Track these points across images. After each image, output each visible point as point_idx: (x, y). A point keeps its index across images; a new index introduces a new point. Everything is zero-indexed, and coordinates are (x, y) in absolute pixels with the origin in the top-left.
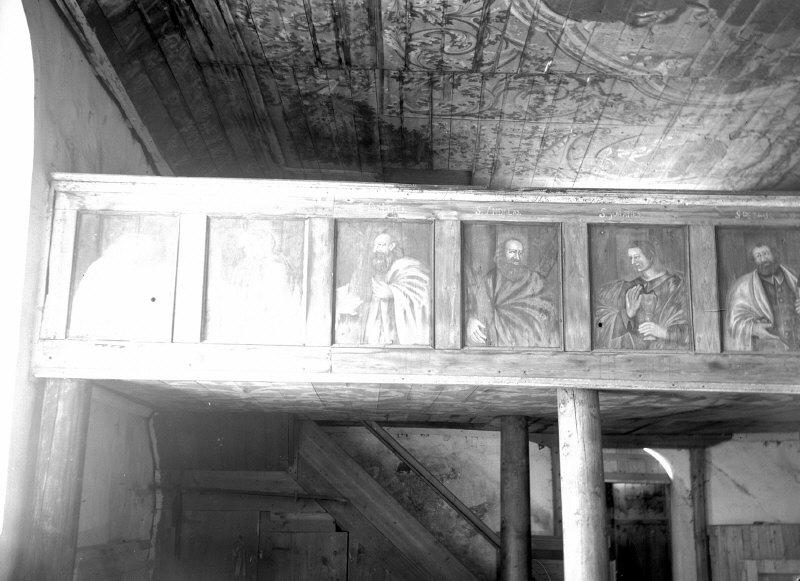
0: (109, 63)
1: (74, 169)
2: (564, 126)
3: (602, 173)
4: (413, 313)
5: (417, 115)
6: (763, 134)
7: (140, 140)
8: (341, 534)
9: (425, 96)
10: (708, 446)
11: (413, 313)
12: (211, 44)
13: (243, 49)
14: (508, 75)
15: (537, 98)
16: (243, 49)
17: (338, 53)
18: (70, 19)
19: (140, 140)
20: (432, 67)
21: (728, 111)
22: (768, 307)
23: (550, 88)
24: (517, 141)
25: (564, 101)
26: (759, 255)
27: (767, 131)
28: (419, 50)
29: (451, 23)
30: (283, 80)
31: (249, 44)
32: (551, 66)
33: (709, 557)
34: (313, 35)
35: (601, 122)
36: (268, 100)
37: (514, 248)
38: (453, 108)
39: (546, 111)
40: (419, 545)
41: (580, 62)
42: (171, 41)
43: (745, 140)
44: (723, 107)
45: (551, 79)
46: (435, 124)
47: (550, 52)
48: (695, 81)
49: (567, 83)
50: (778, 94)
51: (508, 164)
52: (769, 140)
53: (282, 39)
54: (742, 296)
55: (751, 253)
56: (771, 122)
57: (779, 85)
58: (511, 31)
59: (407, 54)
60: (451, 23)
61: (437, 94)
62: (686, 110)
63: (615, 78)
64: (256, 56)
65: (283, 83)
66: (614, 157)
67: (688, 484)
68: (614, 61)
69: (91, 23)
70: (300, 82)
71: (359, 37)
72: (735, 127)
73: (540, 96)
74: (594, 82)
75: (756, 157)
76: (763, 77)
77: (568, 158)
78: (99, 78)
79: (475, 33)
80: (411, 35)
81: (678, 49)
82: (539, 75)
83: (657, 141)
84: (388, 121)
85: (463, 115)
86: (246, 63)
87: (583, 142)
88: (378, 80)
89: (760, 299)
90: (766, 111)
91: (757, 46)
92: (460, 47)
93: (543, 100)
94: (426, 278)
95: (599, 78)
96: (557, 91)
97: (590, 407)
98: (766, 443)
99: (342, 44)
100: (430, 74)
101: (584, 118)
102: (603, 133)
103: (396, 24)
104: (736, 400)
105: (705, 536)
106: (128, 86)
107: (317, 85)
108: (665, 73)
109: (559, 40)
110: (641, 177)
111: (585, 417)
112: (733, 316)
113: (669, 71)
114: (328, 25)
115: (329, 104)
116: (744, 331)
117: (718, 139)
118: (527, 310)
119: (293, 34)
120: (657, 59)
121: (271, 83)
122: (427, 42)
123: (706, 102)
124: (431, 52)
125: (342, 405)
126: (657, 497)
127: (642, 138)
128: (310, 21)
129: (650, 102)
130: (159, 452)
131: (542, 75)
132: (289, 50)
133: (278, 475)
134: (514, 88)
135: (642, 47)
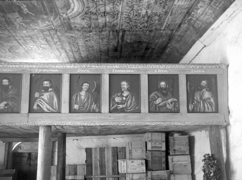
98: (73, 140)
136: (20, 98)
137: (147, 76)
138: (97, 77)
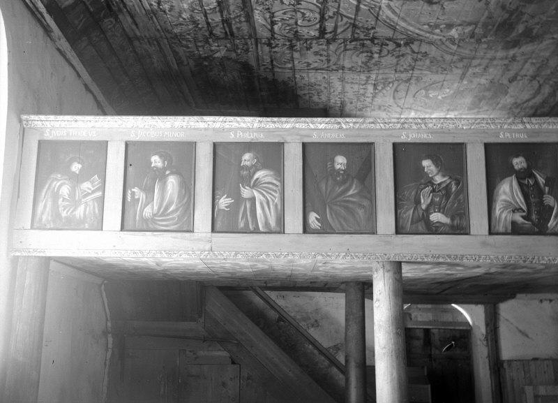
0: (65, 39)
1: (39, 113)
2: (389, 76)
3: (420, 108)
4: (270, 212)
5: (284, 71)
6: (534, 78)
7: (91, 92)
8: (235, 366)
9: (288, 56)
10: (498, 303)
11: (270, 212)
12: (136, 25)
13: (159, 27)
14: (345, 40)
15: (367, 56)
16: (159, 27)
17: (224, 28)
18: (34, 10)
19: (91, 92)
20: (291, 35)
21: (506, 62)
22: (523, 201)
23: (376, 49)
24: (356, 87)
25: (386, 58)
26: (517, 164)
27: (536, 76)
28: (280, 24)
29: (300, 4)
30: (188, 47)
31: (162, 23)
32: (374, 33)
33: (500, 383)
34: (206, 16)
35: (415, 72)
36: (180, 62)
37: (340, 161)
38: (309, 64)
39: (375, 65)
40: (291, 374)
41: (395, 30)
42: (108, 23)
43: (521, 82)
44: (502, 59)
45: (376, 42)
46: (297, 76)
47: (373, 23)
48: (479, 41)
49: (388, 45)
50: (540, 49)
51: (351, 103)
52: (539, 82)
53: (184, 19)
54: (505, 193)
55: (512, 161)
56: (538, 69)
57: (541, 42)
58: (344, 9)
59: (272, 28)
60: (300, 4)
61: (296, 55)
62: (475, 62)
63: (421, 41)
64: (168, 31)
65: (188, 50)
66: (427, 96)
67: (483, 330)
68: (420, 29)
69: (49, 12)
70: (200, 49)
71: (237, 17)
72: (512, 73)
73: (369, 54)
74: (406, 44)
75: (531, 95)
76: (529, 36)
77: (394, 98)
78: (59, 50)
79: (318, 10)
80: (273, 13)
81: (464, 19)
82: (366, 39)
83: (456, 85)
84: (264, 75)
85: (316, 69)
86: (161, 37)
87: (403, 87)
88: (254, 46)
89: (517, 195)
90: (534, 61)
91: (522, 14)
92: (309, 21)
93: (371, 57)
94: (278, 183)
95: (410, 41)
96: (381, 51)
97: (395, 273)
98: (541, 301)
99: (226, 22)
100: (290, 41)
101: (402, 70)
102: (417, 79)
103: (262, 7)
104: (504, 268)
105: (497, 365)
106: (80, 55)
107: (212, 51)
108: (456, 36)
109: (378, 14)
110: (448, 110)
111: (391, 280)
112: (498, 208)
113: (459, 35)
114: (215, 8)
115: (222, 64)
116: (506, 218)
117: (500, 82)
118: (351, 206)
119: (191, 15)
120: (450, 26)
121: (181, 51)
122: (285, 18)
123: (489, 56)
124: (289, 25)
125: (230, 275)
126: (463, 336)
127: (445, 82)
128: (202, 6)
129: (448, 57)
130: (108, 305)
131: (369, 40)
132: (190, 27)
133: (193, 325)
134: (350, 49)
135: (438, 19)
136: (192, 193)
137: (483, 148)
138: (102, 146)
